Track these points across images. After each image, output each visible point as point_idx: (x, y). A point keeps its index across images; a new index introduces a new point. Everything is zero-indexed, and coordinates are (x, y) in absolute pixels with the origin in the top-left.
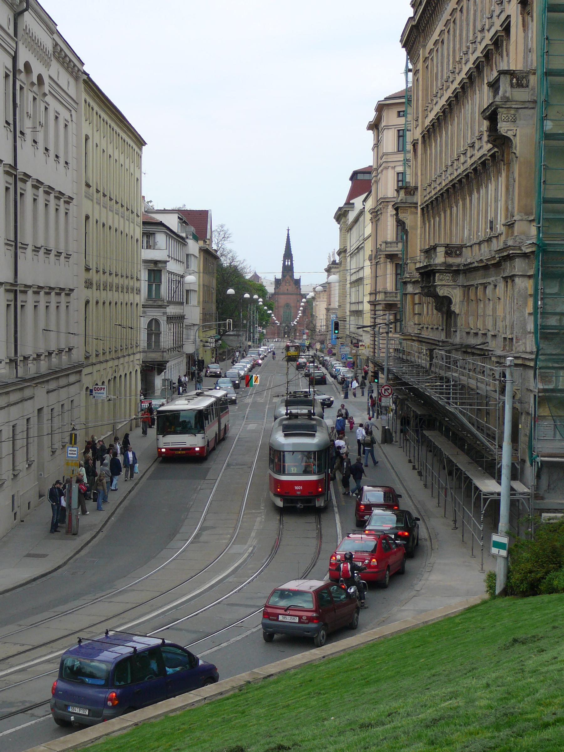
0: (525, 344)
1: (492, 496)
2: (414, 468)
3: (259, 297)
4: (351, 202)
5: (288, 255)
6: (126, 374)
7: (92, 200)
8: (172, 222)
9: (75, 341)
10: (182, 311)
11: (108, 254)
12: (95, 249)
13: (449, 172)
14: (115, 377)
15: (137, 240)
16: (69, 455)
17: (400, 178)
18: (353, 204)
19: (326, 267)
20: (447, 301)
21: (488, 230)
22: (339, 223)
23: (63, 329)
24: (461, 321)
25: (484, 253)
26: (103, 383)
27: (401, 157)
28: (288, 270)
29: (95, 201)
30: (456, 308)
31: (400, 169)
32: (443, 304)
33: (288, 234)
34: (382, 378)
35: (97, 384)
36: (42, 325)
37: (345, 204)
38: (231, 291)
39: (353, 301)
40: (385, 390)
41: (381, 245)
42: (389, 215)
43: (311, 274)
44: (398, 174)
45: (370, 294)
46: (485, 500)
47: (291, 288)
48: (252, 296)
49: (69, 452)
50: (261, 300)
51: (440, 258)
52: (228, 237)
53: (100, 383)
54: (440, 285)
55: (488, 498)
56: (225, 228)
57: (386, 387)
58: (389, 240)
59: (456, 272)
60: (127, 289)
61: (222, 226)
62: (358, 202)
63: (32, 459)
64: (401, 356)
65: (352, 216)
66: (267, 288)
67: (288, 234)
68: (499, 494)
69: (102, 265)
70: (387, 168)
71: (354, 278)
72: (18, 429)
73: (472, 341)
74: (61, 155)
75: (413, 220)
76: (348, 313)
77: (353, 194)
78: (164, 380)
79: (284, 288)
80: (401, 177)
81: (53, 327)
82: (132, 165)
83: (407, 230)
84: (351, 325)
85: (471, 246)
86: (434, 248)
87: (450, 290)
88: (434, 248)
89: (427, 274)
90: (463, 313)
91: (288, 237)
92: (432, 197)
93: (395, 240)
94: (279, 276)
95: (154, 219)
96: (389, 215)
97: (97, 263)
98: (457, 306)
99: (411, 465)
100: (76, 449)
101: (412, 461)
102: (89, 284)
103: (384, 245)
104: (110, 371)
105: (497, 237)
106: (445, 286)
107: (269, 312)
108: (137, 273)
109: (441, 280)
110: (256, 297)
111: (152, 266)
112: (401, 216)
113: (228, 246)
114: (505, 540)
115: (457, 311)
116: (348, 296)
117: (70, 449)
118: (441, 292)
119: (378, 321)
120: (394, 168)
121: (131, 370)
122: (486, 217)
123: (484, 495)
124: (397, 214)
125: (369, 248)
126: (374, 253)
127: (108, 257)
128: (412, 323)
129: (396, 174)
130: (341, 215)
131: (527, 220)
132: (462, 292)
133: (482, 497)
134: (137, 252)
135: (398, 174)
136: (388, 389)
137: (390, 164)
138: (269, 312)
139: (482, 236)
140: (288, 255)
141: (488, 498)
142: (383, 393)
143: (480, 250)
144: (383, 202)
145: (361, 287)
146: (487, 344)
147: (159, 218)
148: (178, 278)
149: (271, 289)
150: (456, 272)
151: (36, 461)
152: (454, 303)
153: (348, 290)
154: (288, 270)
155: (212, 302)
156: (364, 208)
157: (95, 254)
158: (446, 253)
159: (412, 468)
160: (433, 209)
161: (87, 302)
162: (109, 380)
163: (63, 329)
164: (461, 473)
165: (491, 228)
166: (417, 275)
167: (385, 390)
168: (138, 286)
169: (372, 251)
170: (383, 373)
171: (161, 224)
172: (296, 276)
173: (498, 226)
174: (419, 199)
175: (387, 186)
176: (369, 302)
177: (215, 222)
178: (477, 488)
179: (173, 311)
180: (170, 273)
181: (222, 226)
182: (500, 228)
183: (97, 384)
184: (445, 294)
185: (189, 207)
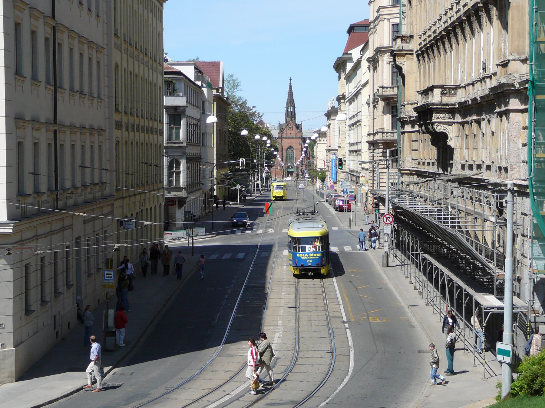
0: (519, 172)
1: (493, 310)
2: (415, 288)
3: (268, 139)
4: (349, 52)
5: (291, 102)
6: (151, 208)
7: (121, 51)
8: (189, 72)
9: (106, 177)
10: (199, 152)
11: (135, 98)
12: (123, 95)
13: (443, 21)
14: (142, 210)
15: (160, 88)
16: (106, 278)
17: (395, 30)
18: (351, 54)
19: (326, 112)
20: (444, 136)
21: (481, 71)
22: (337, 72)
23: (96, 166)
24: (457, 155)
25: (480, 91)
26: (132, 215)
27: (397, 10)
28: (291, 115)
29: (123, 51)
30: (451, 143)
31: (397, 21)
32: (440, 140)
33: (291, 84)
34: (383, 209)
35: (126, 217)
36: (78, 162)
37: (344, 54)
38: (244, 132)
39: (352, 142)
40: (387, 218)
41: (378, 90)
42: (385, 62)
43: (310, 120)
44: (393, 25)
45: (369, 135)
46: (486, 314)
47: (294, 132)
48: (261, 137)
49: (106, 275)
50: (269, 141)
51: (436, 97)
52: (237, 86)
53: (129, 215)
54: (436, 122)
55: (489, 312)
56: (234, 78)
57: (387, 216)
58: (385, 85)
59: (451, 110)
60: (152, 131)
61: (231, 76)
62: (355, 53)
63: (71, 283)
64: (398, 189)
65: (349, 66)
66: (272, 132)
67: (291, 84)
68: (502, 308)
69: (129, 109)
70: (383, 20)
71: (353, 121)
72: (32, 269)
73: (468, 173)
74: (93, 8)
75: (409, 65)
76: (348, 153)
77: (351, 45)
78: (186, 213)
79: (287, 132)
80: (396, 27)
81: (88, 164)
82: (154, 19)
83: (404, 74)
84: (351, 164)
85: (465, 87)
86: (431, 89)
87: (446, 126)
88: (431, 89)
89: (425, 114)
90: (458, 147)
91: (291, 86)
92: (427, 44)
93: (390, 85)
94: (283, 121)
95: (173, 69)
96: (385, 62)
97: (125, 107)
98: (453, 141)
99: (412, 286)
100: (112, 273)
101: (413, 282)
102: (118, 125)
103: (381, 90)
104: (138, 204)
105: (490, 77)
106: (440, 123)
107: (275, 153)
108: (160, 116)
109: (438, 118)
110: (265, 138)
111: (172, 112)
112: (399, 61)
113: (238, 94)
114: (509, 348)
115: (453, 146)
116: (347, 137)
117: (106, 272)
118: (439, 129)
119: (375, 158)
120: (389, 20)
121: (156, 204)
122: (480, 59)
123: (485, 309)
124: (394, 60)
125: (366, 93)
126: (372, 97)
127: (135, 100)
128: (410, 159)
129: (391, 25)
130: (340, 65)
131: (520, 60)
132: (457, 129)
133: (483, 311)
134: (160, 97)
135: (393, 25)
136: (389, 218)
137: (384, 17)
138: (275, 153)
139: (474, 76)
140: (291, 102)
141: (489, 312)
142: (385, 221)
143: (473, 89)
144: (379, 51)
145: (359, 129)
146: (482, 174)
147: (178, 68)
148: (195, 122)
149: (275, 133)
150: (451, 110)
151: (75, 284)
152: (449, 138)
153: (347, 133)
154: (291, 115)
155: (225, 144)
156: (362, 57)
157: (123, 97)
158: (442, 94)
159: (413, 288)
160: (428, 55)
161: (118, 142)
162: (137, 213)
163: (96, 166)
164: (461, 291)
165: (484, 69)
166: (415, 114)
167: (387, 218)
168: (161, 128)
169: (369, 95)
170: (384, 205)
171: (180, 73)
172: (298, 122)
173: (491, 67)
174: (414, 45)
175: (382, 37)
176: (367, 142)
177: (227, 70)
178: (478, 304)
179: (191, 152)
180: (189, 117)
181: (231, 76)
182: (492, 68)
183: (126, 217)
184: (441, 131)
185: (201, 60)
